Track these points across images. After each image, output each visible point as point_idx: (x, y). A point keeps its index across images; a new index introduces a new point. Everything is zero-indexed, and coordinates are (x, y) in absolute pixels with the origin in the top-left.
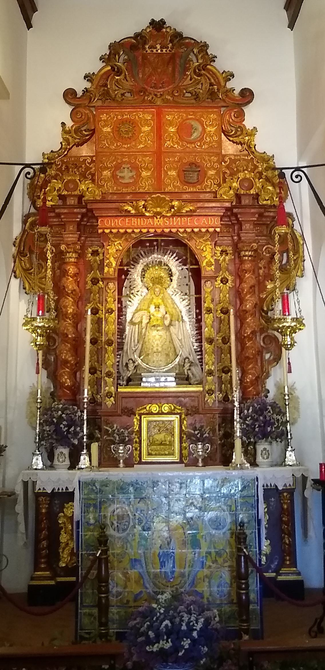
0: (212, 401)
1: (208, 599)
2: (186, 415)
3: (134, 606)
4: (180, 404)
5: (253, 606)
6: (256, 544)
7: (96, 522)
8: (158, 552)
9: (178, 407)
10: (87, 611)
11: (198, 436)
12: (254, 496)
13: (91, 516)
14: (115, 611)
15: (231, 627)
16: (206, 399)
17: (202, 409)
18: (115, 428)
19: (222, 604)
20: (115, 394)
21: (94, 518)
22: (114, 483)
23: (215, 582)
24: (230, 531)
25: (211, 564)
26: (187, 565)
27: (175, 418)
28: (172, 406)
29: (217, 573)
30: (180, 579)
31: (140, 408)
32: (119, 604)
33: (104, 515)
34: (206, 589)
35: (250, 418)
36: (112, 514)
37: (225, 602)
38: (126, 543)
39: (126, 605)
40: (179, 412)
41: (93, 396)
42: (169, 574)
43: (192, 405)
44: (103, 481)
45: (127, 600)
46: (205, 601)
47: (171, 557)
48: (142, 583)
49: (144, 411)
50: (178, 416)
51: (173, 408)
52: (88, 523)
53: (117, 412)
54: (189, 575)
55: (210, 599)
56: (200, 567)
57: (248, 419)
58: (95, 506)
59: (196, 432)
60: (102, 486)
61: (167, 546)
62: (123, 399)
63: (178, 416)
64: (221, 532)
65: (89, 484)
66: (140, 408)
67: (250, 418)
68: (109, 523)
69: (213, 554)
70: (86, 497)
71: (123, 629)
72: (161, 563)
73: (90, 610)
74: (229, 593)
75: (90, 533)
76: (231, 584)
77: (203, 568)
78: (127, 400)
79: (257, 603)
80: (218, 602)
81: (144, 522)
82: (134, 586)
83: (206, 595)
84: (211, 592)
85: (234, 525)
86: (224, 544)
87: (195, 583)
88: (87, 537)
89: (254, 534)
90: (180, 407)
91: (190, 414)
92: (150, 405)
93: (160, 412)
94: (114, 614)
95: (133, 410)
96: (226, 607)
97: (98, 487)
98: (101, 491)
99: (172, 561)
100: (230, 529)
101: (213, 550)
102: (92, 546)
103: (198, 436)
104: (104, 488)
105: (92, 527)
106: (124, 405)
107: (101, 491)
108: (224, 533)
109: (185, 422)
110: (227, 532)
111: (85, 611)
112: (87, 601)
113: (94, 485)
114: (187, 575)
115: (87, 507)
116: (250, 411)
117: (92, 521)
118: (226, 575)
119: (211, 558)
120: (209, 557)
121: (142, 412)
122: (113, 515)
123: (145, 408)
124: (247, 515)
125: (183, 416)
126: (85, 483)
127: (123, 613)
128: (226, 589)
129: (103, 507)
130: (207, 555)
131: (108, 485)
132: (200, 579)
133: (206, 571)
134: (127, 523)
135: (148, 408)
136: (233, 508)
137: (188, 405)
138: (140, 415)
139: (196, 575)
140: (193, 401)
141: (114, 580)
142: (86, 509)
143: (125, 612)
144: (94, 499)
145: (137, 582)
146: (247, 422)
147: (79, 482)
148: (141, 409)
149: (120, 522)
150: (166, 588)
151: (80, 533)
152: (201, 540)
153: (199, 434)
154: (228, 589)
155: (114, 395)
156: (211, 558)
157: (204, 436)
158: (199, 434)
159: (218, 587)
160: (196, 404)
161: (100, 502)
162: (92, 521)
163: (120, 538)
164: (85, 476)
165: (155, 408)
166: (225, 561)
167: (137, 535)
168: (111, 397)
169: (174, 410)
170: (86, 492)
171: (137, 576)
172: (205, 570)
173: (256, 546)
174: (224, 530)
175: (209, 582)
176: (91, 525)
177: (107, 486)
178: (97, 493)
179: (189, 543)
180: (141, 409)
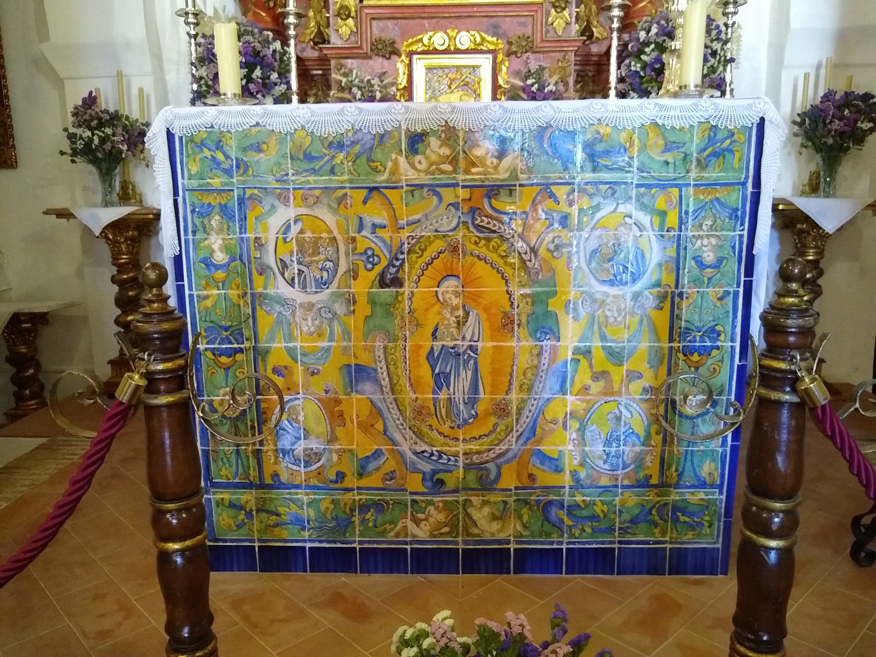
0: (564, 25)
1: (574, 474)
2: (509, 54)
3: (359, 488)
4: (495, 31)
5: (707, 494)
6: (734, 327)
7: (233, 259)
8: (427, 344)
9: (489, 38)
10: (226, 495)
11: (534, 89)
12: (744, 184)
13: (216, 242)
14: (305, 499)
15: (638, 543)
16: (550, 19)
17: (542, 41)
18: (354, 76)
19: (616, 486)
20: (356, 11)
21: (226, 249)
22: (282, 137)
23: (597, 433)
24: (655, 290)
25: (589, 382)
26: (515, 385)
27: (485, 63)
28: (477, 35)
29: (607, 408)
30: (493, 420)
31: (411, 40)
32: (314, 482)
33: (256, 238)
34: (570, 447)
35: (652, 46)
36: (281, 236)
37: (626, 482)
38: (331, 320)
39: (337, 486)
40: (492, 47)
41: (319, 29)
42: (462, 406)
43: (520, 33)
44: (245, 134)
45: (338, 473)
46: (566, 480)
47: (466, 363)
48: (381, 429)
49: (419, 47)
50: (490, 56)
51: (478, 40)
52: (208, 263)
53: (360, 48)
54: (520, 411)
55: (583, 474)
56: (557, 387)
57: (647, 50)
58: (224, 209)
59: (529, 82)
60: (245, 150)
61: (455, 331)
62: (374, 23)
63: (490, 56)
64: (629, 291)
65: (202, 144)
66: (411, 40)
67: (652, 46)
68: (273, 264)
69: (599, 356)
70: (194, 183)
71: (328, 542)
72: (437, 377)
73: (231, 494)
74: (639, 461)
75: (215, 292)
76: (648, 436)
77: (565, 393)
78: (381, 24)
79: (720, 487)
80: (605, 481)
81: (384, 262)
82: (357, 434)
83: (570, 463)
84: (584, 456)
85: (671, 272)
86: (635, 325)
87: (538, 430)
88: (209, 303)
89: (729, 300)
90: (495, 39)
91: (515, 53)
92: (431, 34)
93: (452, 48)
94: (301, 507)
95: (396, 46)
96: (628, 493)
97: (233, 155)
98: (241, 166)
99: (470, 373)
100: (658, 284)
101: (596, 344)
102: (226, 329)
103: (534, 89)
104: (252, 157)
105: (220, 275)
106: (376, 34)
107: (241, 166)
108: (636, 296)
109: (504, 69)
110: (646, 292)
111: (218, 496)
112: (223, 473)
113: (219, 147)
114: (514, 411)
115: (201, 215)
116: (654, 30)
117: (220, 257)
118: (634, 415)
119: (591, 366)
120: (584, 363)
121: (414, 48)
122: (285, 239)
123: (421, 40)
124: (714, 241)
125: (500, 57)
126: (191, 139)
127: (325, 504)
128: (630, 450)
129: (251, 216)
130: (580, 357)
131: (264, 147)
132: (554, 422)
133: (572, 401)
134: (329, 264)
135: (426, 41)
136: (672, 219)
137: (510, 34)
138: (410, 54)
139: (541, 411)
140: (523, 25)
141: (297, 421)
142: (198, 222)
143: (333, 501)
144: (219, 192)
145: (366, 427)
146: (644, 57)
147: (170, 136)
148: (412, 44)
149: (307, 259)
150: (452, 443)
151: (187, 292)
152: (561, 316)
153: (536, 86)
154: (637, 449)
155: (353, 14)
156: (591, 366)
157: (546, 91)
158: (536, 86)
159: (608, 443)
160: (528, 31)
161: (241, 201)
162: (220, 257)
163: (310, 307)
164: (186, 117)
165: (439, 40)
166: (633, 375)
167: (362, 300)
168: (348, 16)
169: (481, 44)
170: (194, 170)
171: (365, 411)
172: (570, 398)
173: (733, 333)
174: (637, 287)
175: (582, 430)
176: (218, 267)
177: (259, 150)
178: (228, 172)
179: (524, 321)
180: (412, 44)
